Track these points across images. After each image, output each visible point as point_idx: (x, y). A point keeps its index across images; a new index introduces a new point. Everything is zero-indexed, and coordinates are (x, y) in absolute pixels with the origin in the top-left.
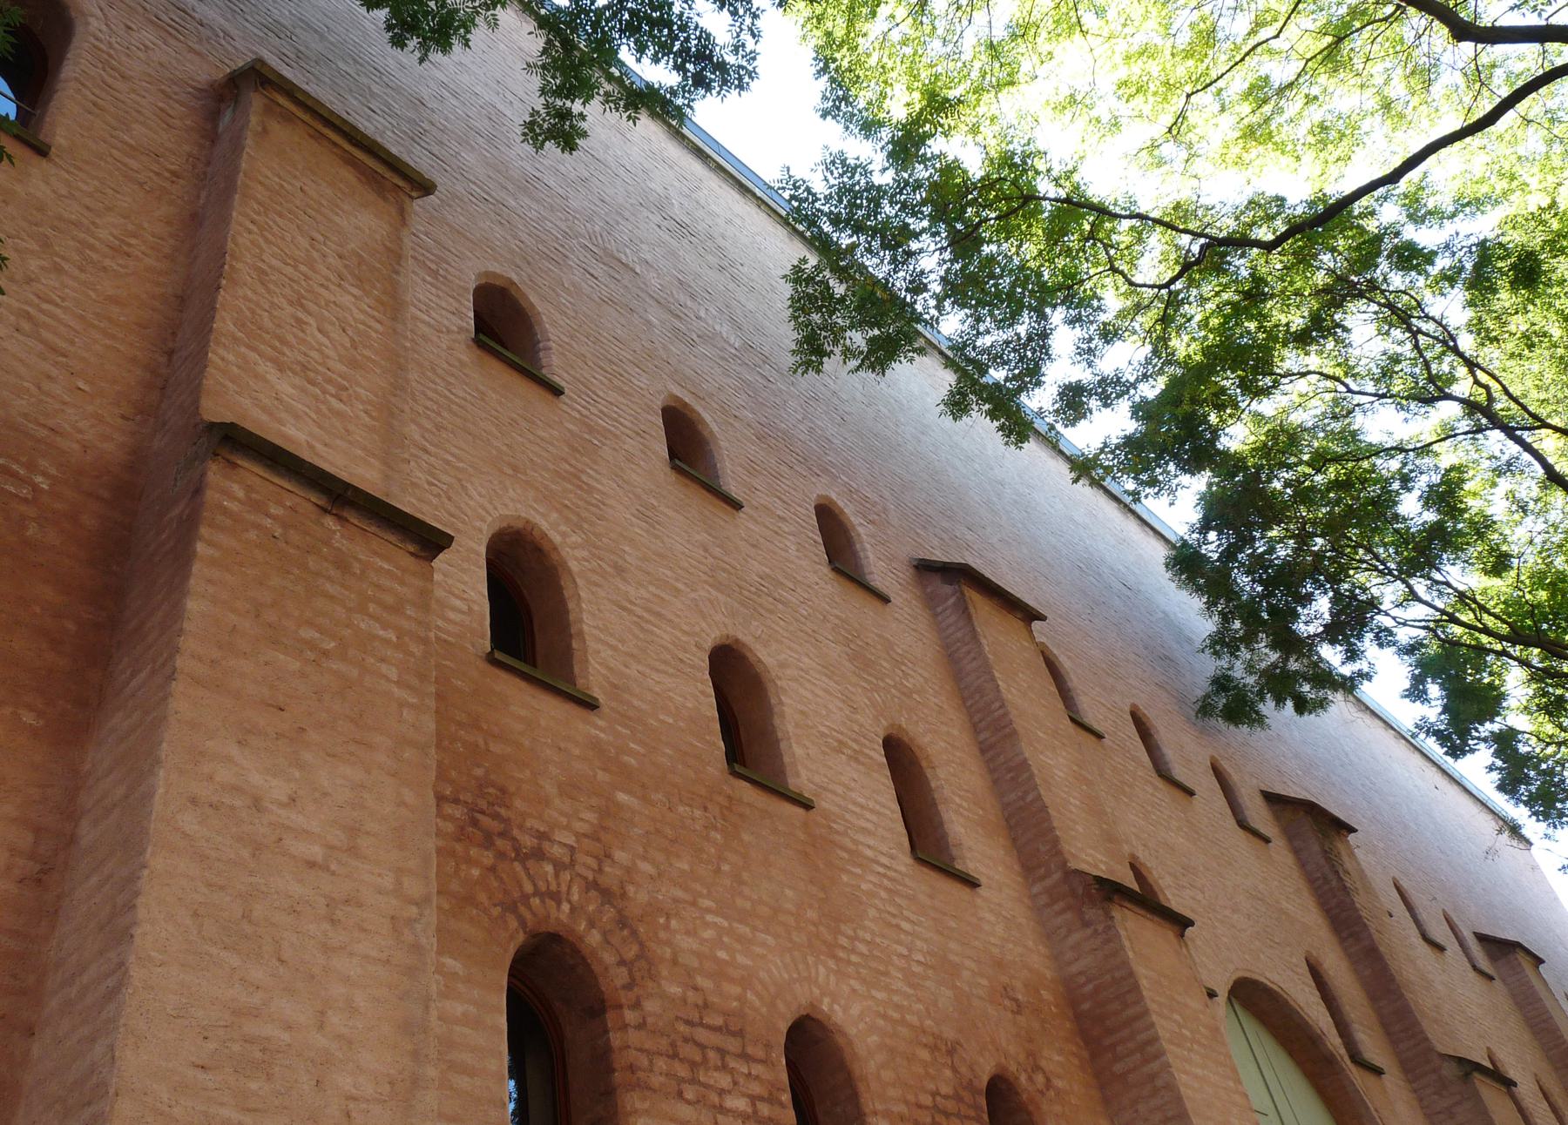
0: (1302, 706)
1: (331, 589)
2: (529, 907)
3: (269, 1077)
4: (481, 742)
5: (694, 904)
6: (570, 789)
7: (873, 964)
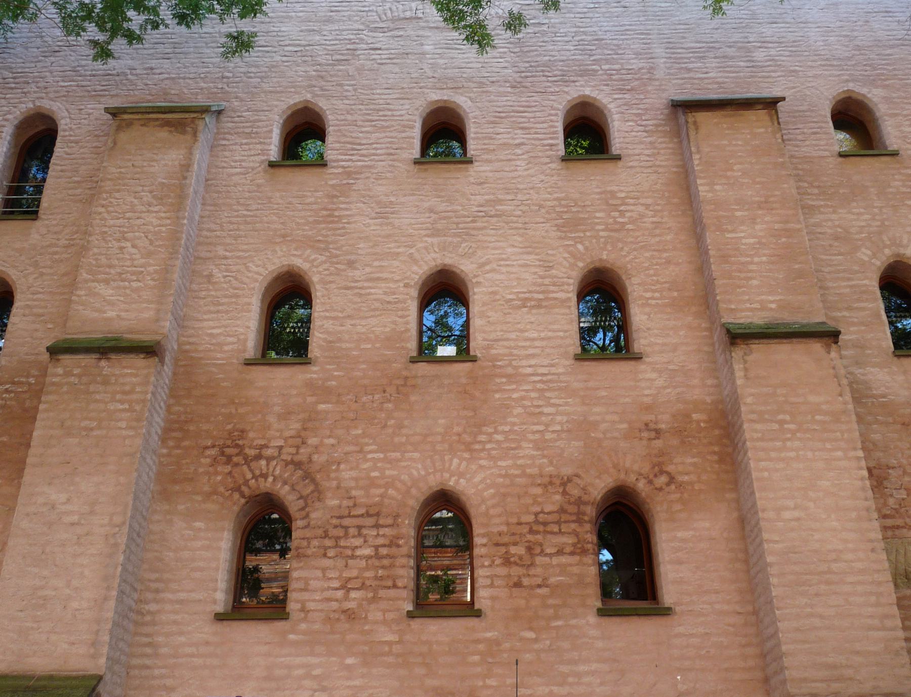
4: (233, 411)
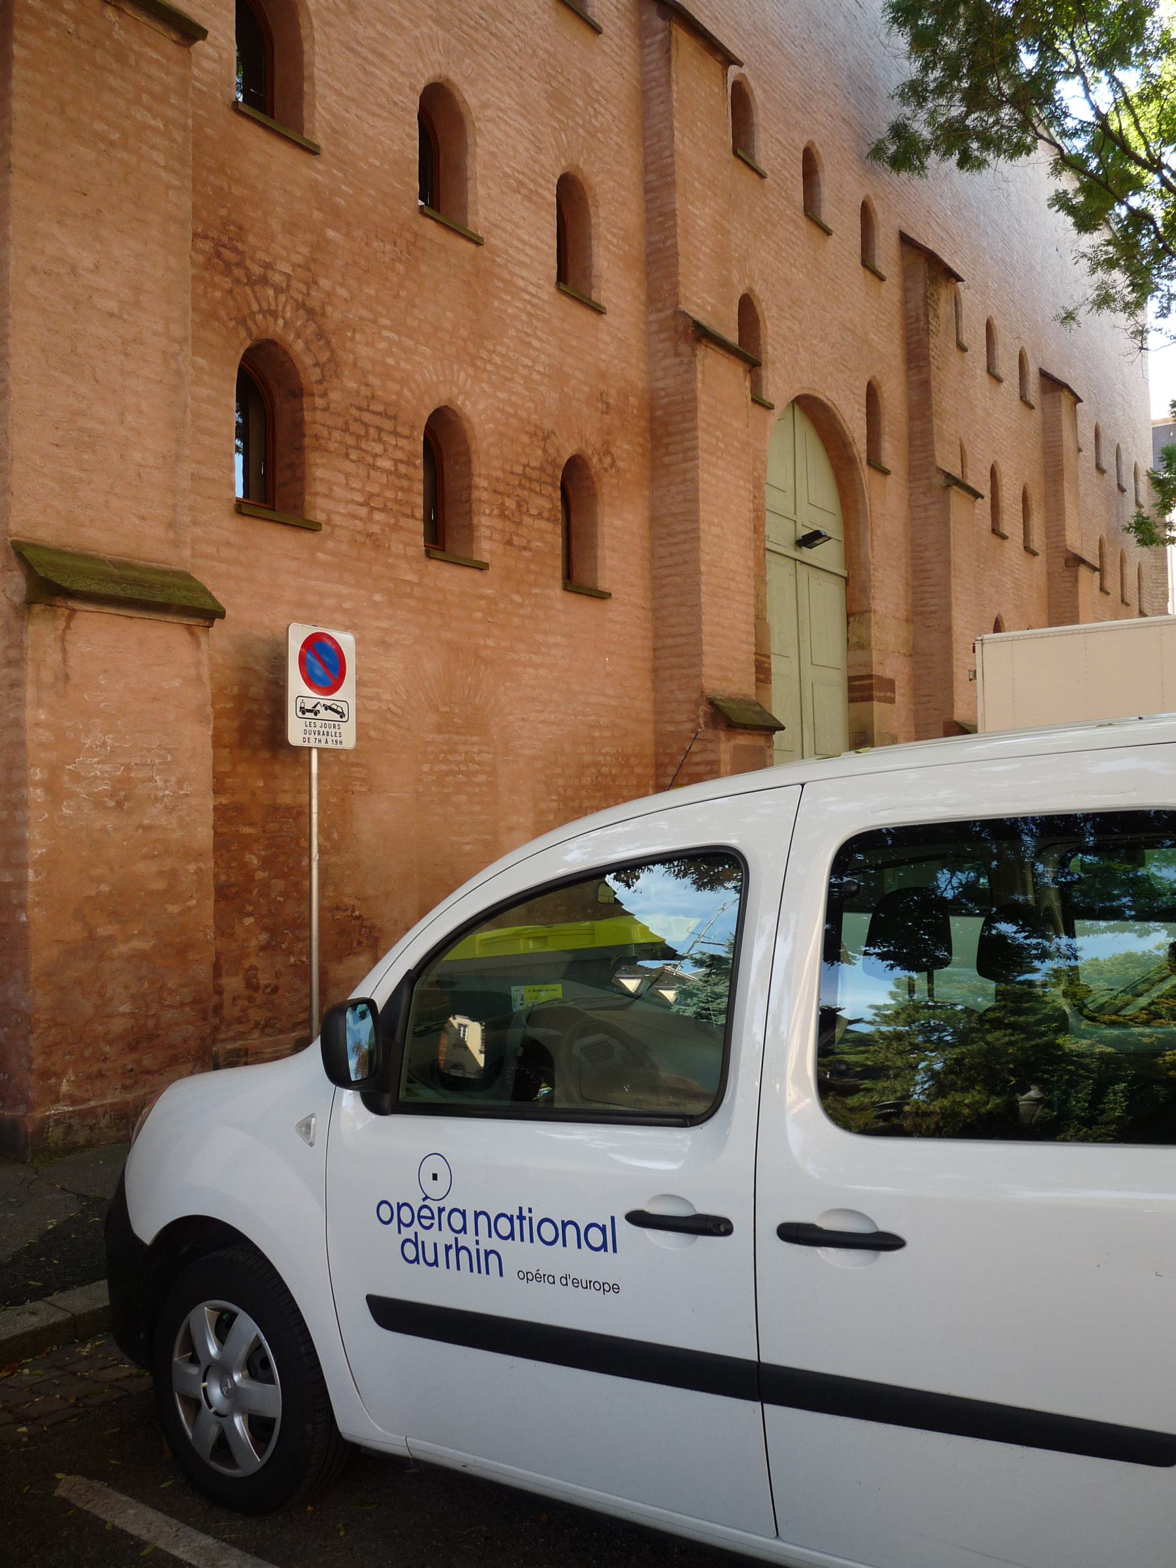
0: (966, 161)
1: (114, 82)
2: (255, 321)
3: (94, 451)
4: (225, 185)
5: (375, 322)
6: (291, 227)
7: (503, 372)
